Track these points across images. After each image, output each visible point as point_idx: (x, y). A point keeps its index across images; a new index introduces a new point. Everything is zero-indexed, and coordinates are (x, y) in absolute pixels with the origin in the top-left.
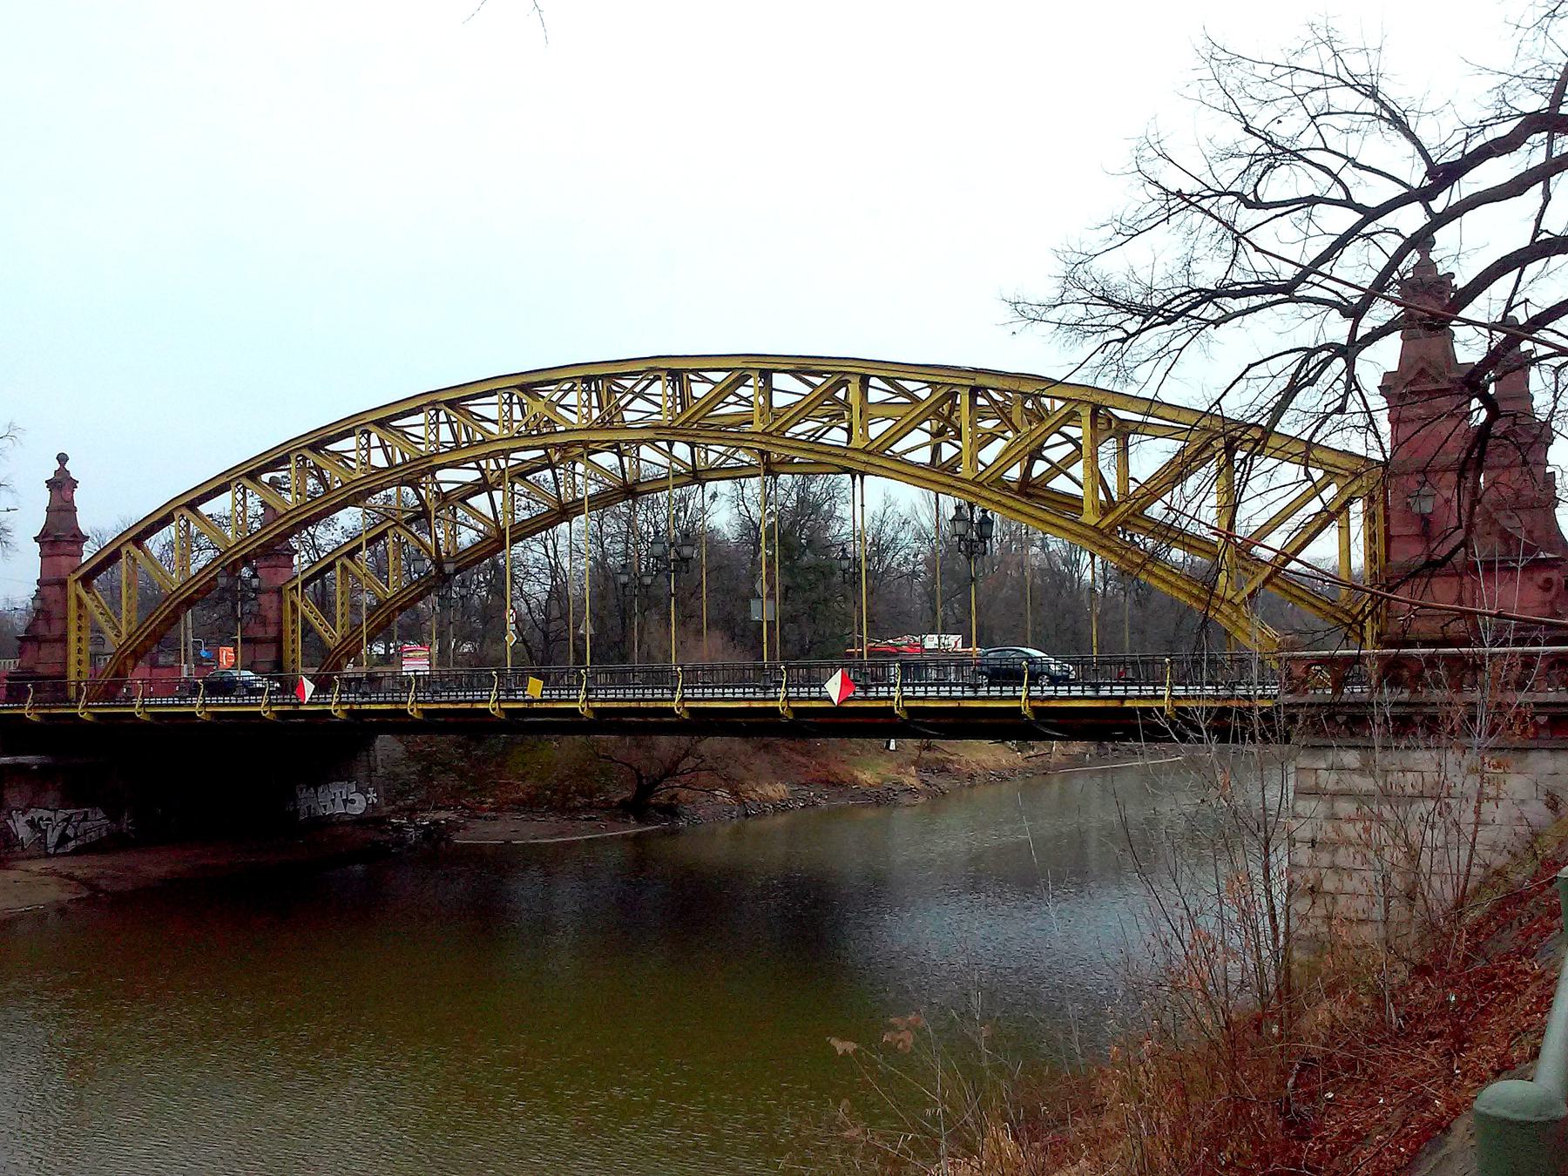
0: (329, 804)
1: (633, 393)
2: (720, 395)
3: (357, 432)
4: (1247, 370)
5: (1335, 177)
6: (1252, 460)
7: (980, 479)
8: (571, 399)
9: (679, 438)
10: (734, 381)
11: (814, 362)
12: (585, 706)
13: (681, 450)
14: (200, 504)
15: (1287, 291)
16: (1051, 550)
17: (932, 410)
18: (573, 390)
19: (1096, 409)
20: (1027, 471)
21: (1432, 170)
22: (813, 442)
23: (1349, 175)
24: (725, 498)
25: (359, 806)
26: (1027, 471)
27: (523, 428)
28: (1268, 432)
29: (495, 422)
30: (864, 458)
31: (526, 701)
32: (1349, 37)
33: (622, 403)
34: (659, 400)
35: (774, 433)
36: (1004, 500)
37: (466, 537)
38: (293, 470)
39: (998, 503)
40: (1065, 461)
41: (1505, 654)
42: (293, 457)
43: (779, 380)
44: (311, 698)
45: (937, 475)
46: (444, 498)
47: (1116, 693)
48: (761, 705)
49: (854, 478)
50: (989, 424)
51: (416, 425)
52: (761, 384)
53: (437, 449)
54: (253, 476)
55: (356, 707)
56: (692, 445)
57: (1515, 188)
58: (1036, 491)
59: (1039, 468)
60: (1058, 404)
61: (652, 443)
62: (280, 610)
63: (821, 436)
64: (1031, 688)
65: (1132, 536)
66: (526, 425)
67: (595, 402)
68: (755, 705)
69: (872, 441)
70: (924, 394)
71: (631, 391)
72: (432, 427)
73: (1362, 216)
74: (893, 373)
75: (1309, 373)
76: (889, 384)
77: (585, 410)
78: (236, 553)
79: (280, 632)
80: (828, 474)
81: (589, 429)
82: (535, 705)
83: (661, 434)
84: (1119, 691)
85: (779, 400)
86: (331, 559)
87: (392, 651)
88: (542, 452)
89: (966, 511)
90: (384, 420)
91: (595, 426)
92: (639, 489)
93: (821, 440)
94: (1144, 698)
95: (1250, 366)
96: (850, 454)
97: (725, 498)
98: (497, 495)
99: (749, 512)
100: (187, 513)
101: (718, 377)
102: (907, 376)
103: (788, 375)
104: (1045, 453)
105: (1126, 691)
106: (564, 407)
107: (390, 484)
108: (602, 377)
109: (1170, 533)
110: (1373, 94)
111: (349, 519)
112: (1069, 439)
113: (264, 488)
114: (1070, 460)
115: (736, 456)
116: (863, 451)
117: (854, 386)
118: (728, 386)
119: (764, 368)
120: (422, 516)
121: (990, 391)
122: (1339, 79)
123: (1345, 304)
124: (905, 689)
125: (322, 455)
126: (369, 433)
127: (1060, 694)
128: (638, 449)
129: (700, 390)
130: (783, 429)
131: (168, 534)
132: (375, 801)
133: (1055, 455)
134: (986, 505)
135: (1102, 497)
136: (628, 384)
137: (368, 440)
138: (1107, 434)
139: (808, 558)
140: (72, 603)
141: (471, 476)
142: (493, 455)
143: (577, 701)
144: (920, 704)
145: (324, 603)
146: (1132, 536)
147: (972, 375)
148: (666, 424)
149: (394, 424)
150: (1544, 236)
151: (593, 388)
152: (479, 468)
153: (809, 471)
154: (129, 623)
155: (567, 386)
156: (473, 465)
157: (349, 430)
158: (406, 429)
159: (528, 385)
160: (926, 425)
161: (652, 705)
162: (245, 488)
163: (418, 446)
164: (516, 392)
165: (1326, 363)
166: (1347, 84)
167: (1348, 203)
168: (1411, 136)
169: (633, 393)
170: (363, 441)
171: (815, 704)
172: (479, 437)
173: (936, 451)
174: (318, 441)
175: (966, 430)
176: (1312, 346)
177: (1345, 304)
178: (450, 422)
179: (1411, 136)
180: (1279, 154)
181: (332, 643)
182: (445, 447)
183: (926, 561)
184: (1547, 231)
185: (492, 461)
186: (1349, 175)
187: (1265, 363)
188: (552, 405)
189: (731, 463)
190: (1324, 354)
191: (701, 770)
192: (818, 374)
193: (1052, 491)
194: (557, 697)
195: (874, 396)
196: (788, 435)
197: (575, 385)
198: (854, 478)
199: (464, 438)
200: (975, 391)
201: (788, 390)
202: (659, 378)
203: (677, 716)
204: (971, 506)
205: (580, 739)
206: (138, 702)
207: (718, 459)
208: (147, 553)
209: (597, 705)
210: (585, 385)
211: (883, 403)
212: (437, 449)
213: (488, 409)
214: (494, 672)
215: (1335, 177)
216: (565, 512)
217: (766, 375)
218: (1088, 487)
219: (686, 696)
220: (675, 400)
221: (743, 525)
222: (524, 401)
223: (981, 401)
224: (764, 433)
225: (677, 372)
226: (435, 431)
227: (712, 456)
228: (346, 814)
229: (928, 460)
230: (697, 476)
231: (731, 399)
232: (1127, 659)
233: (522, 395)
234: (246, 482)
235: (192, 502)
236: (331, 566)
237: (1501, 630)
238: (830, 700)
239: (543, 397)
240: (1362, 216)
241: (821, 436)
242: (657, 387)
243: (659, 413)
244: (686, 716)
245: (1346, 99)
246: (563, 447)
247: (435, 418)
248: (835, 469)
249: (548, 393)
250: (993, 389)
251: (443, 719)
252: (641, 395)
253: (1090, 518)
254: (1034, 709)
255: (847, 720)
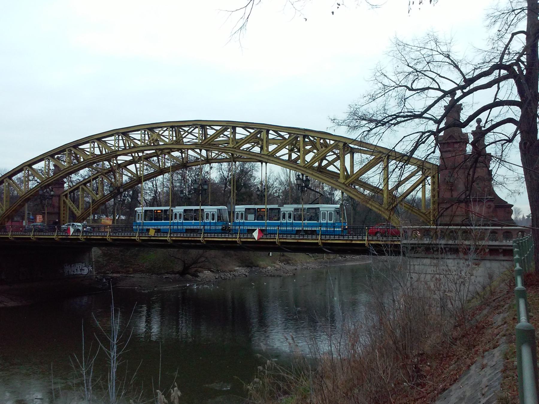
0: (75, 271)
1: (188, 132)
2: (218, 133)
3: (90, 142)
4: (403, 138)
5: (433, 80)
6: (405, 166)
7: (306, 166)
8: (166, 133)
9: (203, 148)
10: (224, 129)
11: (250, 124)
12: (169, 239)
13: (204, 153)
14: (33, 165)
15: (420, 116)
16: (325, 190)
17: (290, 142)
18: (167, 130)
19: (345, 144)
20: (320, 164)
21: (465, 80)
22: (248, 151)
23: (438, 79)
24: (215, 169)
25: (86, 271)
26: (320, 164)
27: (149, 143)
28: (410, 157)
29: (139, 140)
30: (267, 157)
31: (149, 237)
32: (441, 38)
33: (183, 136)
34: (197, 135)
35: (237, 148)
36: (314, 173)
37: (125, 179)
38: (67, 154)
39: (312, 174)
40: (333, 161)
41: (479, 229)
42: (67, 150)
43: (238, 130)
44: (72, 234)
45: (290, 164)
46: (119, 165)
47: (350, 238)
48: (231, 240)
49: (262, 164)
50: (308, 147)
51: (111, 141)
52: (232, 131)
53: (118, 149)
54: (52, 156)
55: (89, 237)
56: (207, 151)
57: (489, 85)
58: (323, 170)
59: (325, 163)
60: (332, 142)
61: (193, 149)
62: (59, 203)
63: (251, 149)
64: (322, 236)
65: (354, 186)
66: (150, 142)
67: (174, 135)
68: (229, 240)
69: (270, 152)
70: (287, 136)
71: (187, 131)
72: (117, 141)
73: (443, 94)
74: (277, 129)
75: (422, 140)
76: (276, 133)
77: (171, 137)
78: (45, 183)
79: (59, 210)
80: (251, 162)
81: (172, 144)
82: (152, 238)
83: (194, 146)
84: (351, 238)
85: (238, 137)
86: (77, 186)
87: (96, 218)
88: (154, 151)
89: (301, 177)
90: (99, 138)
91: (174, 143)
92: (188, 165)
93: (251, 151)
94: (345, 240)
95: (404, 137)
96: (262, 156)
97: (215, 169)
98: (138, 165)
99: (223, 173)
100: (28, 168)
101: (218, 128)
102: (282, 130)
103: (241, 129)
104: (327, 158)
105: (353, 238)
106: (163, 136)
107: (101, 160)
108: (177, 126)
109: (366, 185)
110: (448, 57)
111: (84, 172)
112: (335, 154)
113: (56, 160)
114: (335, 160)
115: (222, 155)
116: (267, 155)
117: (264, 132)
118: (221, 131)
119: (233, 126)
120: (112, 170)
121: (310, 137)
122: (437, 51)
123: (435, 119)
124: (280, 235)
125: (77, 149)
126: (94, 143)
127: (331, 238)
128: (188, 151)
129: (211, 132)
130: (240, 146)
131: (20, 175)
132: (92, 270)
133: (330, 158)
134: (308, 175)
135: (346, 174)
136: (186, 129)
137: (94, 145)
138: (347, 152)
139: (243, 190)
140: (62, 202)
141: (128, 158)
142: (138, 152)
143: (135, 236)
144: (285, 241)
145: (75, 201)
146: (354, 186)
147: (304, 131)
148: (199, 143)
149: (103, 140)
150: (497, 100)
151: (174, 130)
152: (132, 156)
153: (245, 161)
154: (6, 206)
155: (165, 129)
156: (130, 155)
157: (88, 141)
158: (107, 142)
159: (150, 128)
160: (287, 147)
161: (193, 239)
162: (49, 160)
163: (111, 147)
164: (147, 130)
165: (429, 136)
166: (441, 54)
167: (439, 89)
168: (459, 70)
169: (188, 132)
170: (92, 145)
171: (249, 240)
172: (132, 145)
173: (290, 156)
174: (76, 145)
175: (302, 149)
176: (423, 131)
177: (435, 119)
178: (123, 140)
179: (459, 70)
180: (418, 73)
181: (78, 215)
182: (121, 148)
183: (283, 192)
184: (498, 99)
185: (136, 154)
186: (438, 79)
187: (408, 136)
188: (159, 135)
189: (220, 157)
190: (427, 134)
191: (205, 262)
192: (252, 128)
193: (328, 170)
194: (160, 235)
195: (271, 137)
196: (241, 149)
197: (167, 129)
198: (262, 164)
199: (127, 145)
200: (305, 137)
201: (241, 133)
202: (197, 127)
203: (202, 243)
204: (303, 175)
205: (164, 250)
206: (10, 234)
207: (215, 156)
208: (13, 181)
209: (174, 238)
210: (171, 129)
211: (273, 139)
212: (118, 149)
213: (136, 136)
214: (56, 227)
215: (433, 80)
216: (161, 171)
217: (234, 128)
218: (342, 170)
219: (205, 236)
220: (202, 135)
221: (221, 178)
222: (149, 133)
223: (307, 140)
224: (233, 148)
225: (203, 125)
226: (118, 143)
227: (213, 155)
228: (81, 274)
229: (287, 159)
230: (208, 161)
231: (222, 135)
232: (352, 227)
233: (149, 131)
234: (49, 158)
235: (29, 164)
236: (78, 188)
237: (478, 221)
238: (255, 239)
239: (156, 132)
240: (443, 94)
241: (251, 149)
242: (197, 130)
243: (196, 139)
244: (171, 242)
245: (441, 58)
246: (162, 150)
247: (118, 138)
248: (256, 161)
249: (158, 131)
250: (311, 136)
251: (183, 243)
252: (191, 133)
253: (342, 180)
254: (323, 243)
255: (262, 246)
